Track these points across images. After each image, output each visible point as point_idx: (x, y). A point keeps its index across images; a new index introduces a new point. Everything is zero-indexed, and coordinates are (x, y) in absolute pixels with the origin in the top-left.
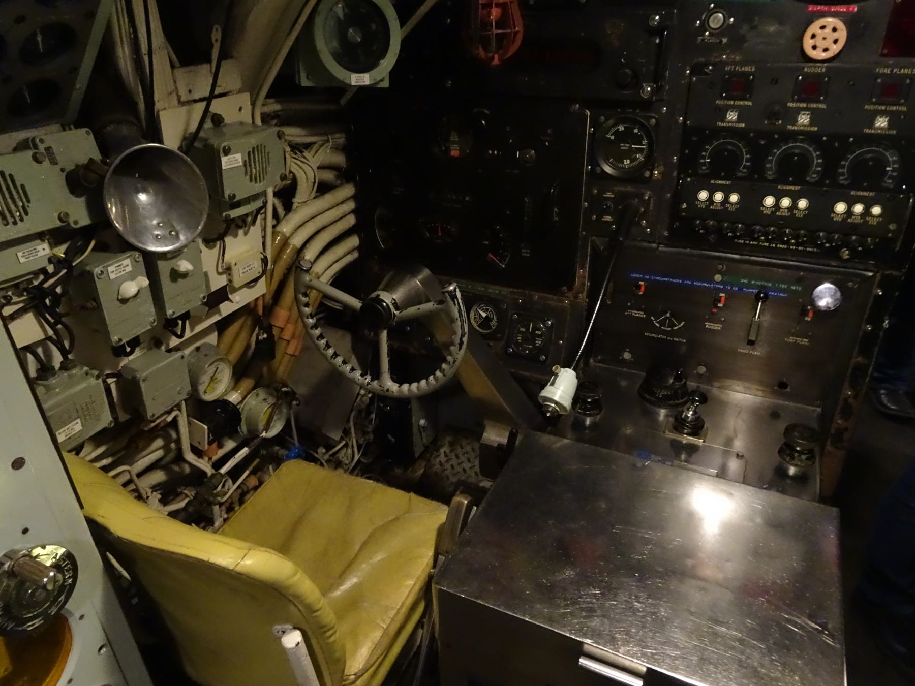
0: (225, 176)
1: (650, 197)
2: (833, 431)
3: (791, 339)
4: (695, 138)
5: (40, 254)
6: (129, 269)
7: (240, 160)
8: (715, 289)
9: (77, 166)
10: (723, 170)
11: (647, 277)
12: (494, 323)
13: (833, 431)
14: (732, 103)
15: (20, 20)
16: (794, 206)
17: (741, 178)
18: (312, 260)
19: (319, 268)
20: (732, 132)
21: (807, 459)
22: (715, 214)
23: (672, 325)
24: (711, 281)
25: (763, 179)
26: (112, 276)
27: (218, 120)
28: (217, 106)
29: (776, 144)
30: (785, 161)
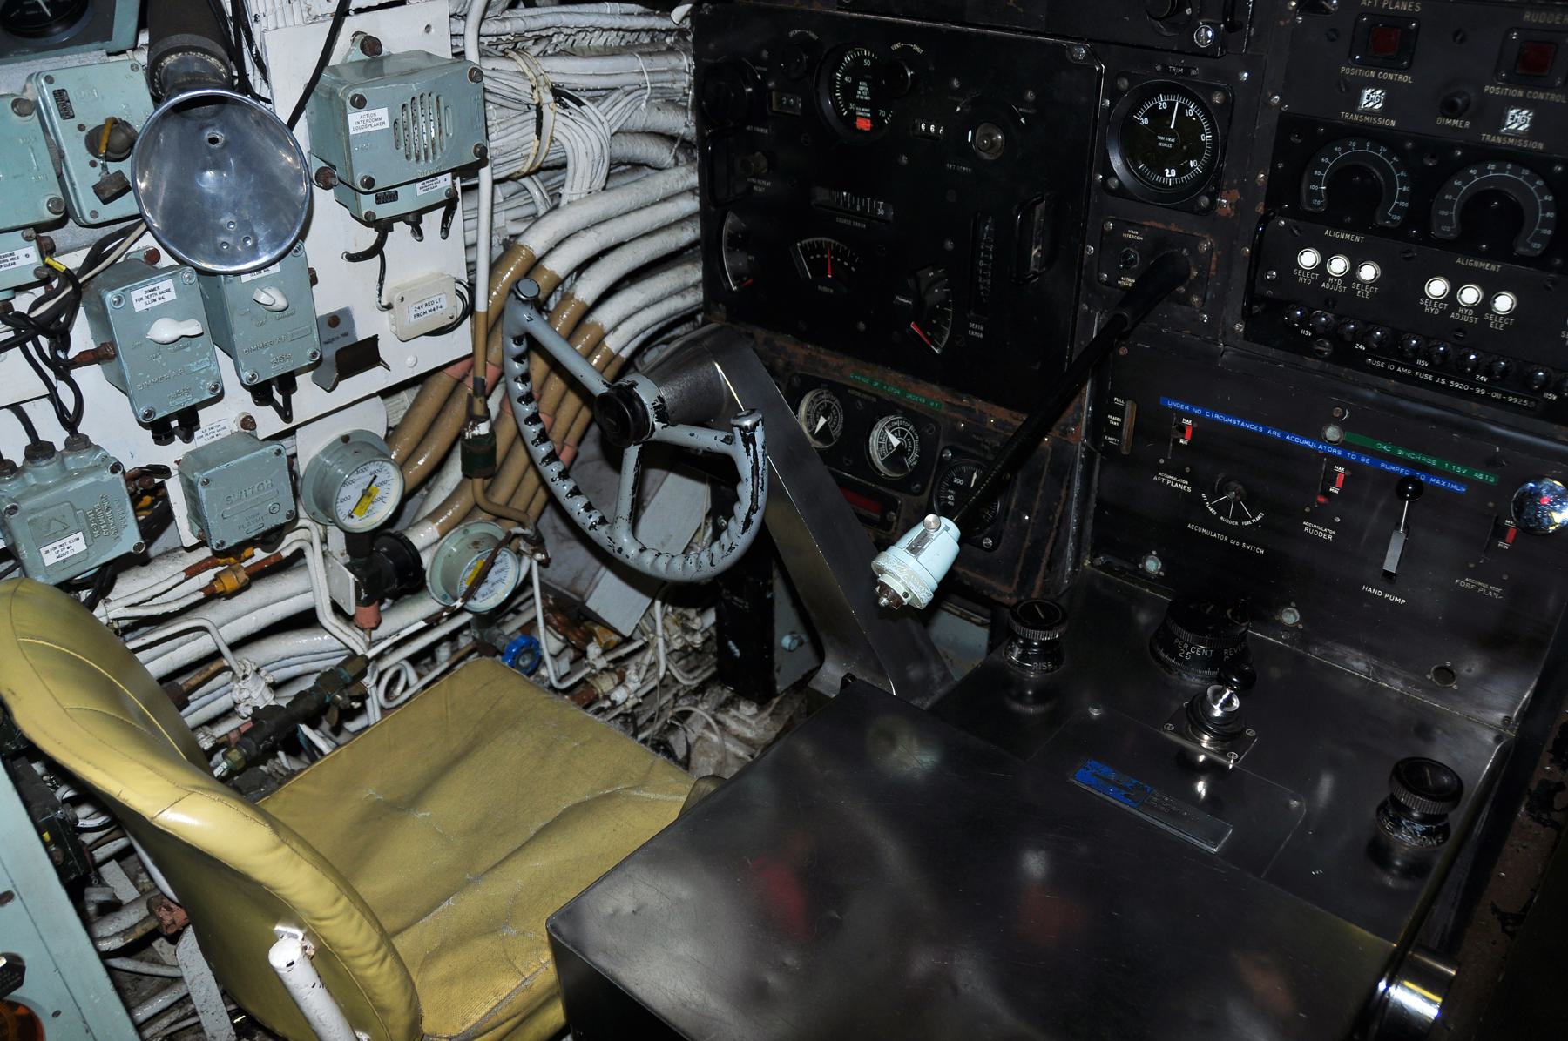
0: (355, 148)
1: (1211, 249)
2: (1533, 786)
3: (1468, 583)
4: (1303, 137)
5: (19, 263)
6: (171, 296)
7: (386, 118)
8: (1326, 454)
10: (1352, 214)
11: (1198, 412)
12: (911, 461)
13: (1533, 786)
14: (1373, 74)
16: (1485, 305)
17: (1384, 232)
18: (589, 302)
19: (606, 316)
20: (1364, 132)
21: (1423, 833)
22: (1330, 301)
25: (1426, 239)
26: (139, 307)
27: (370, 45)
29: (1459, 168)
30: (1339, 179)
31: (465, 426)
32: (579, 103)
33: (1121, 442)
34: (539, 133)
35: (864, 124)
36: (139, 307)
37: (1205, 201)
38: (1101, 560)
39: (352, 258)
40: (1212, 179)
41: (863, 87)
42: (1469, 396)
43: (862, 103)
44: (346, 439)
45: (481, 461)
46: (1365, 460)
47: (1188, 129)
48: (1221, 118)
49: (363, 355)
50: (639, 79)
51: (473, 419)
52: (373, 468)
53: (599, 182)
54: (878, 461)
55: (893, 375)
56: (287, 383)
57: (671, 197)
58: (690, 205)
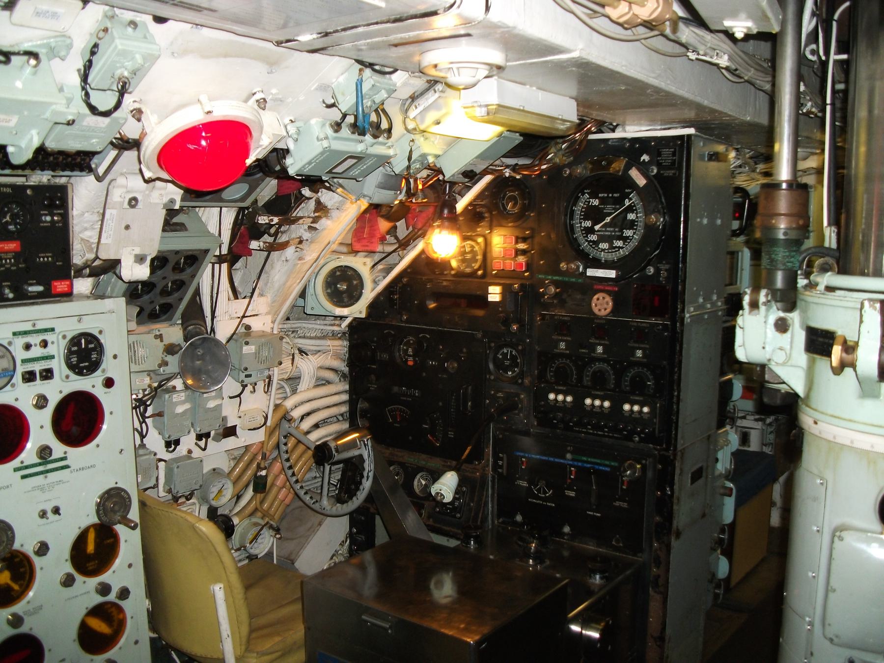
4: (547, 357)
6: (183, 398)
9: (98, 505)
10: (562, 382)
15: (164, 278)
23: (545, 492)
24: (564, 458)
26: (174, 400)
27: (248, 328)
28: (245, 321)
31: (257, 471)
32: (307, 355)
33: (504, 471)
34: (292, 364)
35: (411, 363)
36: (174, 400)
37: (520, 381)
38: (501, 520)
39: (231, 398)
40: (522, 375)
41: (410, 350)
42: (604, 436)
43: (410, 356)
44: (214, 470)
45: (260, 485)
46: (580, 464)
47: (514, 358)
48: (522, 353)
49: (230, 432)
50: (328, 348)
51: (259, 468)
52: (223, 482)
53: (312, 385)
54: (417, 491)
55: (424, 456)
56: (207, 435)
57: (337, 393)
58: (345, 397)
